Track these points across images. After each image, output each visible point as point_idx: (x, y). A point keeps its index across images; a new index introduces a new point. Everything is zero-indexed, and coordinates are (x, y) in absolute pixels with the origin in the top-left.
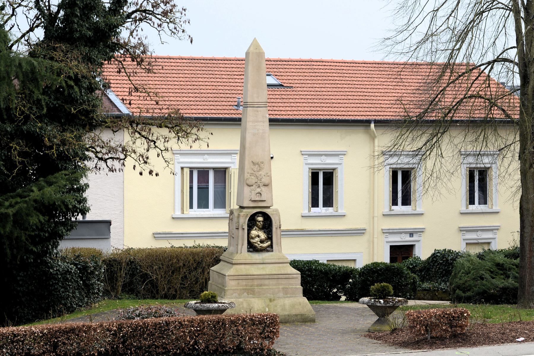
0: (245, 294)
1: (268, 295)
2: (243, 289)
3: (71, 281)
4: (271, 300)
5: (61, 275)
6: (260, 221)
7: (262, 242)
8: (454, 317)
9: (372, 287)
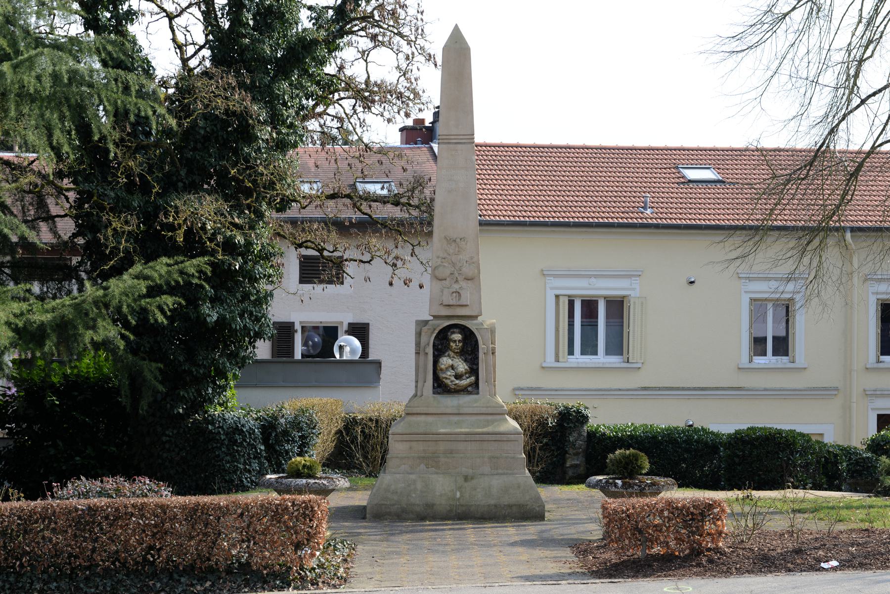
0: (422, 467)
1: (464, 469)
2: (419, 458)
3: (241, 444)
4: (466, 478)
5: (226, 434)
6: (455, 341)
7: (458, 377)
8: (692, 513)
9: (611, 456)
